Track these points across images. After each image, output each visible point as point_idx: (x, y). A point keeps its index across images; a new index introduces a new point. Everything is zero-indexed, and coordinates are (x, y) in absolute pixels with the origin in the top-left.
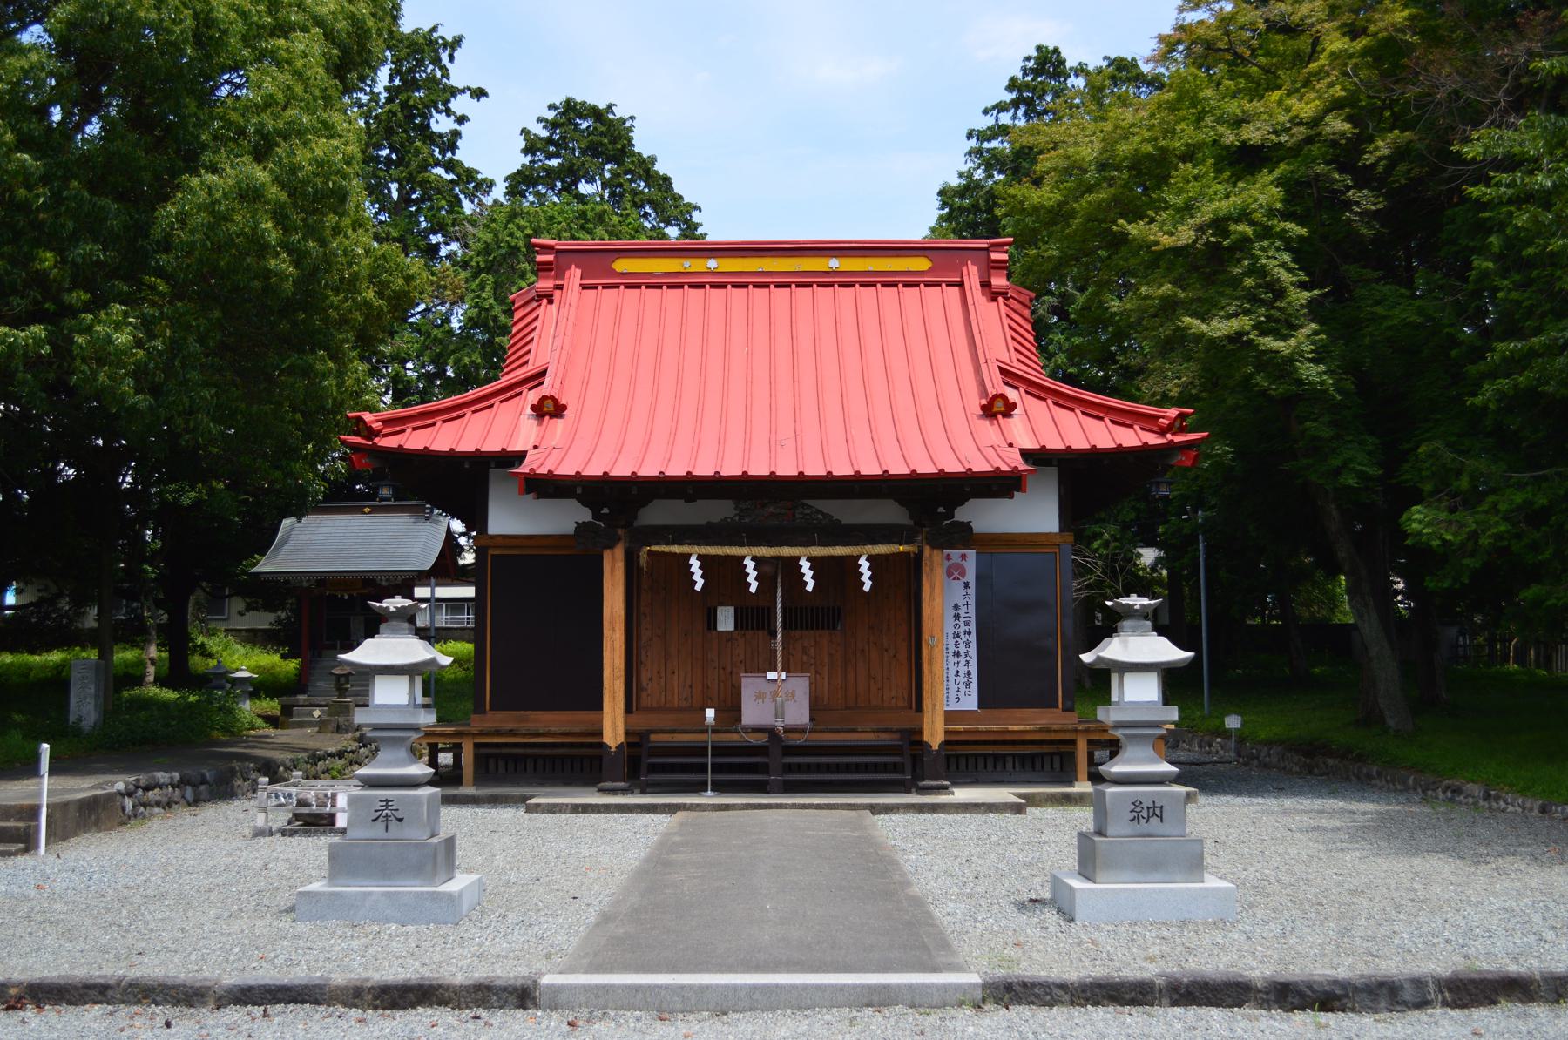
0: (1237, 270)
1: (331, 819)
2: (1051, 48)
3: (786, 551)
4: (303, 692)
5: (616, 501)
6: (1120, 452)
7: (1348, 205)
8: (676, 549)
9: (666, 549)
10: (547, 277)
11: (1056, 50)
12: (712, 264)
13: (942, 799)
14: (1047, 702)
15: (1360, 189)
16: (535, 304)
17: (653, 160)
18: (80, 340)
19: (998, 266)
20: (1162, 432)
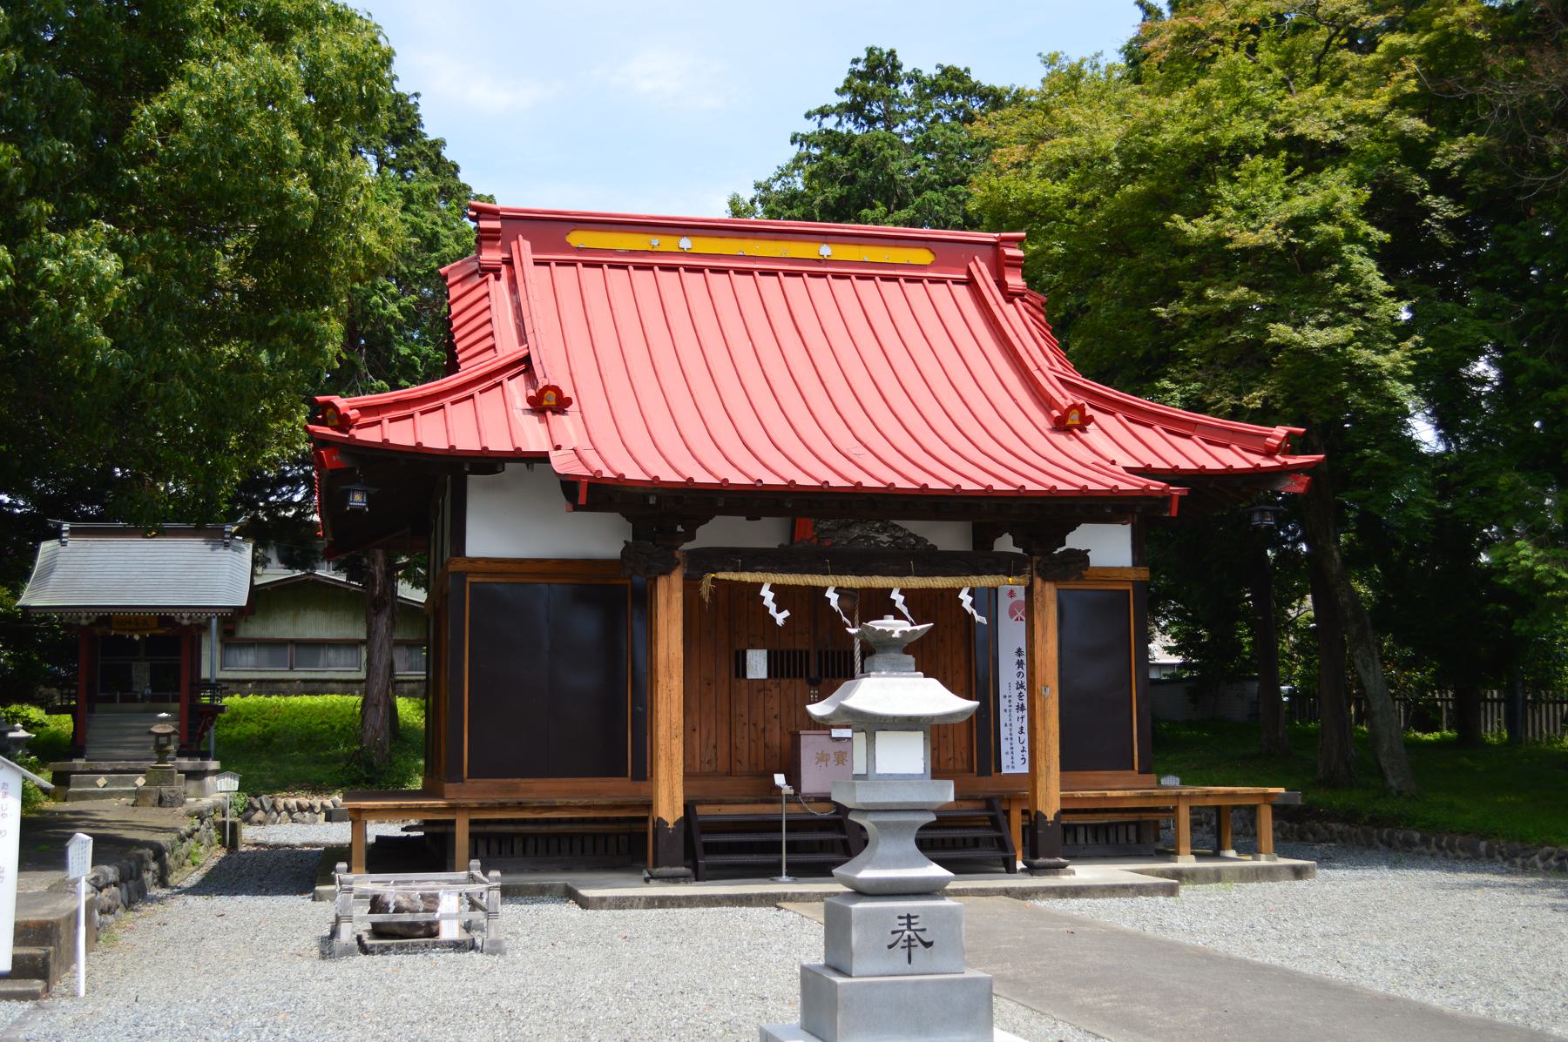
0: (1328, 275)
1: (431, 930)
2: (886, 50)
3: (878, 582)
4: (80, 756)
5: (662, 516)
6: (1229, 473)
7: (1427, 211)
8: (748, 577)
9: (734, 576)
10: (493, 248)
11: (892, 53)
12: (686, 243)
13: (1063, 880)
14: (1121, 762)
15: (1437, 195)
16: (477, 279)
17: (442, 143)
18: (50, 265)
19: (1014, 262)
20: (1269, 453)
